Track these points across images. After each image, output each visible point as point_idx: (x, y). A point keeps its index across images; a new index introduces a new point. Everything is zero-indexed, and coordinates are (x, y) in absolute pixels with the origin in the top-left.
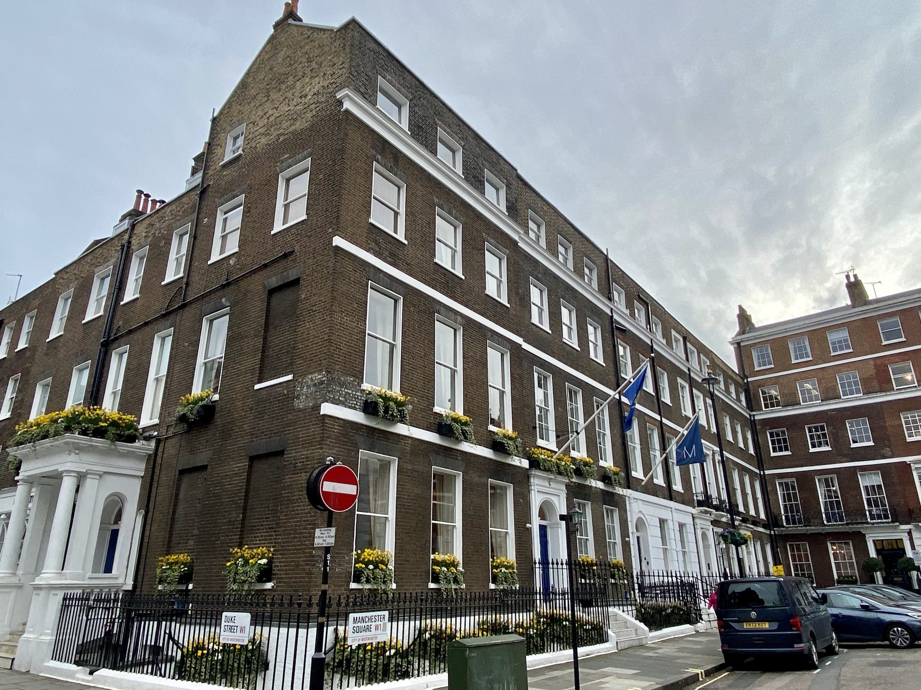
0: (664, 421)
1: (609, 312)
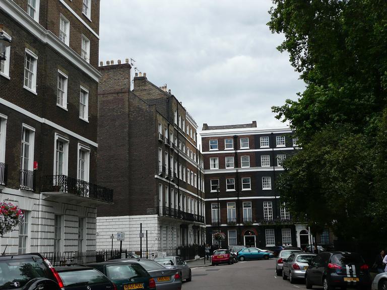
0: (180, 188)
1: (177, 152)
